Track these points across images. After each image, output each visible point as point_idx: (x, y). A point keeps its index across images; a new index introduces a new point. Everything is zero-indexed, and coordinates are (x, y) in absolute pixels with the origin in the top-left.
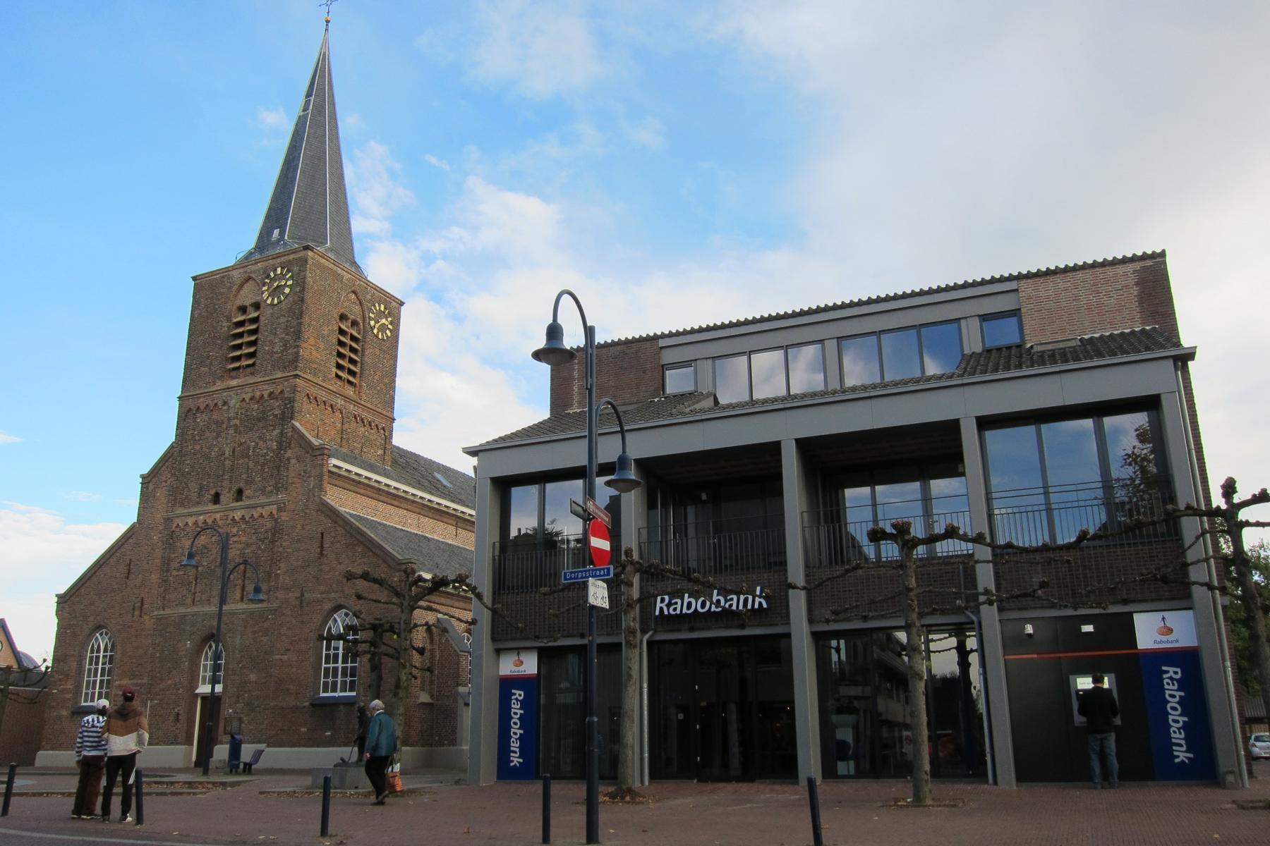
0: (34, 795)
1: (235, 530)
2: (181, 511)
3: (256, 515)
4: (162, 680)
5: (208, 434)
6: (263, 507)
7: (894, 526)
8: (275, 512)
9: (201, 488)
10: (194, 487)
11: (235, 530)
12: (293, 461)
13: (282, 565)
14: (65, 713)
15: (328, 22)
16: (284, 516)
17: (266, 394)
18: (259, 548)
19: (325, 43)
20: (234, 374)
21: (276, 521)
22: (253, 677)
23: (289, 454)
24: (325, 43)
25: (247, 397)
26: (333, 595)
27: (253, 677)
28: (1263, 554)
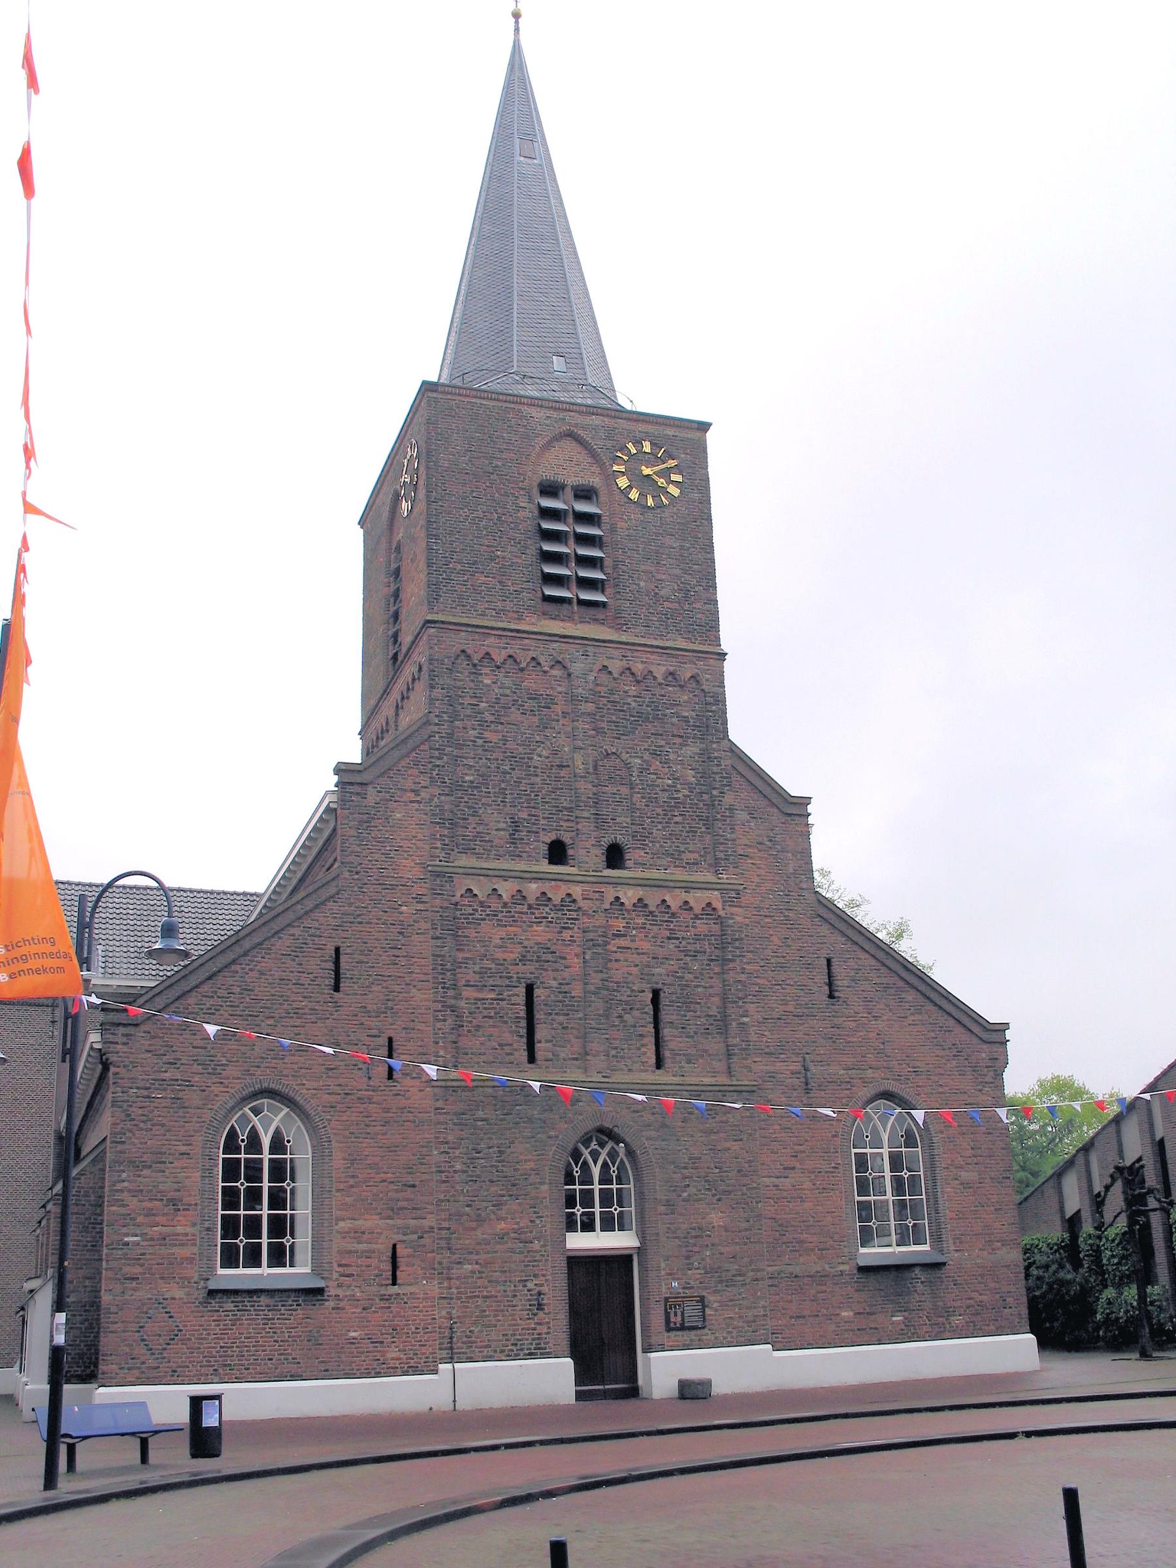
0: (528, 1498)
1: (620, 924)
2: (464, 861)
3: (674, 904)
4: (480, 1220)
5: (515, 715)
6: (687, 889)
7: (64, 1061)
8: (718, 904)
9: (515, 824)
10: (495, 822)
11: (620, 924)
12: (742, 816)
13: (751, 1008)
14: (179, 1293)
15: (517, 16)
16: (739, 916)
17: (659, 672)
18: (685, 967)
19: (517, 50)
20: (551, 608)
21: (720, 921)
22: (716, 1218)
23: (728, 799)
24: (517, 50)
25: (616, 666)
26: (870, 1073)
27: (716, 1218)
28: (616, 1129)
